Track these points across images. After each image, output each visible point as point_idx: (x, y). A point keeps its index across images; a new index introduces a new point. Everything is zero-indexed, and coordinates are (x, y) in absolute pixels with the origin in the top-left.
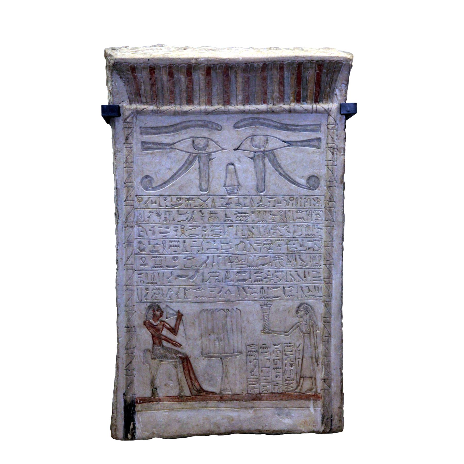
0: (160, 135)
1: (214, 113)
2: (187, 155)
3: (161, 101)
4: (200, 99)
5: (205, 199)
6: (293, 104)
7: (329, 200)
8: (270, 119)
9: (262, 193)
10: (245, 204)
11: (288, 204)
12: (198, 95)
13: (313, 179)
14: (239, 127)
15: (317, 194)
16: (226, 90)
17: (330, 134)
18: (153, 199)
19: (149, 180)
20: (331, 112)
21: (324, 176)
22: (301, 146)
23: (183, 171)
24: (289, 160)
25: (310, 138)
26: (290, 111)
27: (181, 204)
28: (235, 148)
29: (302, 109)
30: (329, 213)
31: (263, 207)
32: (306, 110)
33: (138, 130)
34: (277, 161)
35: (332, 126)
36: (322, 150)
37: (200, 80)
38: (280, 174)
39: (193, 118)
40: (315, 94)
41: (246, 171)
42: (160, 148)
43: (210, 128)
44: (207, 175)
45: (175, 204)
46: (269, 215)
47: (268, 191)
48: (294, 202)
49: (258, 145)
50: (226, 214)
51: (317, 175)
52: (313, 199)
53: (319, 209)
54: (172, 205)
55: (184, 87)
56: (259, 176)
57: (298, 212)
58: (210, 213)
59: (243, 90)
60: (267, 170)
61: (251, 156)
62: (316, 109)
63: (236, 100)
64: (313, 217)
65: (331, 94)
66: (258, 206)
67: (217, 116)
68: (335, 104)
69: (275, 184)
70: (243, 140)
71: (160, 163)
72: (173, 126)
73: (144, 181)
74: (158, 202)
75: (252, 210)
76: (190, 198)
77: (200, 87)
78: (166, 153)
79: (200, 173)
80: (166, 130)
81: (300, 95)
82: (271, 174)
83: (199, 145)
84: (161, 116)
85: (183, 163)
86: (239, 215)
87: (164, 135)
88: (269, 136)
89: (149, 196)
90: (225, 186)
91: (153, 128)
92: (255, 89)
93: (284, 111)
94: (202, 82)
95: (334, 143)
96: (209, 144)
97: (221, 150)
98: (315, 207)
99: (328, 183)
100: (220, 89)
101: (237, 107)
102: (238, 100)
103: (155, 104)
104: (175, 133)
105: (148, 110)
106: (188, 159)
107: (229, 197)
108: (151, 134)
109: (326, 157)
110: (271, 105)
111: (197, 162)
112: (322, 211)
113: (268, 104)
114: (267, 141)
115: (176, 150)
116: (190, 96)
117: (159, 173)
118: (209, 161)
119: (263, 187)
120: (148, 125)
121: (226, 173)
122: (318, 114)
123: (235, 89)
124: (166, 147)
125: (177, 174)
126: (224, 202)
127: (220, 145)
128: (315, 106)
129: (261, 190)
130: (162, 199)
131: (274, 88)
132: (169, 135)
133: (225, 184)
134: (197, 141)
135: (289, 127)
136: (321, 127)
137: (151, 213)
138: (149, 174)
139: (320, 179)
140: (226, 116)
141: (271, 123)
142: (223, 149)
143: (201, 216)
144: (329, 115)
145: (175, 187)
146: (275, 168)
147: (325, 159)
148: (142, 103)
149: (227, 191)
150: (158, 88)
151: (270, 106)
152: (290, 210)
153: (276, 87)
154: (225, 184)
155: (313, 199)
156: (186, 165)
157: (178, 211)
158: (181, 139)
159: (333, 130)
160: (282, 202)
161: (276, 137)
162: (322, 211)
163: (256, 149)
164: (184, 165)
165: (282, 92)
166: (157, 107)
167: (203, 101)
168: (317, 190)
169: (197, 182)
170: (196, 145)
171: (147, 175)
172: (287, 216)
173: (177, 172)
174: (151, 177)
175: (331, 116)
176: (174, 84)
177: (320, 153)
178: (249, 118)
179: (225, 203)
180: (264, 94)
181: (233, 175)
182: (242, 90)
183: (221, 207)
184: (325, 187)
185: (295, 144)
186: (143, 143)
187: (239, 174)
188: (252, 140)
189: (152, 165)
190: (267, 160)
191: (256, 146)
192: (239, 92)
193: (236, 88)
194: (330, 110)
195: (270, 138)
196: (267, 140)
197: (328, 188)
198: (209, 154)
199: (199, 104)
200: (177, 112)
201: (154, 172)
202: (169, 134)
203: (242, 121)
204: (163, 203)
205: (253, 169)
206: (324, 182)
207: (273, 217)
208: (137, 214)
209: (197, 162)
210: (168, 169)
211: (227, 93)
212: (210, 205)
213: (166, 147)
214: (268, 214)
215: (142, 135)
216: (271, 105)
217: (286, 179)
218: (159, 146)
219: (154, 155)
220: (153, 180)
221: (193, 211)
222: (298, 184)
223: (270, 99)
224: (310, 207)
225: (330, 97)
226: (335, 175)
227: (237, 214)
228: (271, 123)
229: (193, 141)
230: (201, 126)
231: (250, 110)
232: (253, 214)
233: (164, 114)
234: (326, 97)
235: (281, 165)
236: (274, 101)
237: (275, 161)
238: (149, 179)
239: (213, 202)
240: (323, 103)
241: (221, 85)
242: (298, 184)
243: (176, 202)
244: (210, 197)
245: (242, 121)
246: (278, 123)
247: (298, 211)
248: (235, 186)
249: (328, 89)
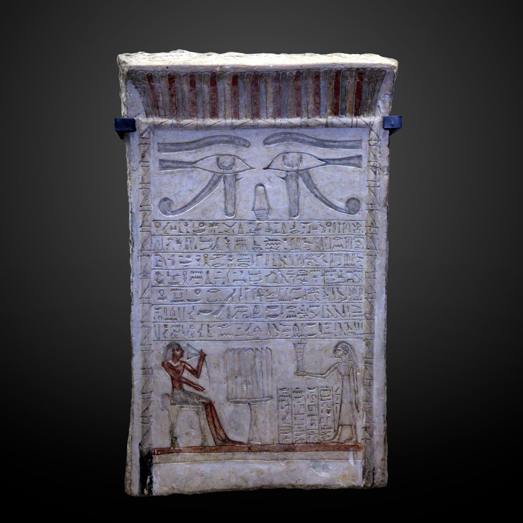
0: (181, 152)
1: (242, 128)
2: (210, 175)
3: (181, 114)
4: (225, 111)
5: (231, 224)
6: (330, 118)
7: (371, 225)
8: (305, 134)
9: (296, 218)
10: (276, 230)
11: (325, 230)
12: (223, 108)
13: (353, 202)
14: (269, 144)
15: (358, 219)
16: (255, 101)
17: (372, 151)
18: (173, 224)
19: (168, 203)
20: (373, 126)
22: (340, 165)
23: (206, 193)
25: (350, 156)
26: (327, 125)
27: (204, 230)
28: (264, 167)
29: (340, 123)
30: (371, 240)
31: (296, 233)
32: (345, 124)
33: (156, 146)
34: (312, 182)
35: (374, 142)
36: (363, 169)
37: (226, 90)
38: (316, 196)
39: (217, 133)
40: (355, 106)
41: (277, 193)
42: (181, 167)
43: (237, 145)
44: (233, 198)
45: (197, 230)
46: (303, 242)
47: (303, 215)
48: (331, 228)
49: (291, 163)
50: (254, 242)
51: (358, 197)
52: (353, 224)
53: (359, 236)
54: (194, 231)
55: (207, 98)
56: (292, 198)
57: (336, 239)
58: (236, 240)
59: (274, 101)
60: (300, 191)
61: (283, 175)
62: (357, 123)
63: (267, 113)
64: (352, 245)
65: (373, 105)
66: (291, 233)
67: (245, 131)
69: (310, 207)
70: (273, 157)
71: (180, 184)
72: (195, 142)
73: (162, 204)
74: (178, 228)
75: (284, 237)
76: (214, 223)
77: (225, 98)
78: (188, 173)
79: (225, 195)
80: (187, 147)
81: (339, 107)
82: (306, 196)
83: (224, 163)
84: (182, 131)
85: (206, 183)
86: (270, 242)
87: (185, 152)
88: (303, 153)
89: (168, 221)
90: (253, 209)
91: (172, 144)
92: (287, 100)
93: (320, 125)
94: (228, 92)
95: (376, 162)
96: (235, 162)
97: (249, 169)
98: (355, 234)
99: (370, 206)
100: (248, 100)
101: (267, 120)
102: (268, 112)
103: (175, 117)
104: (198, 150)
105: (167, 124)
106: (212, 179)
107: (258, 222)
108: (170, 151)
109: (368, 177)
110: (306, 118)
111: (222, 182)
112: (363, 237)
113: (302, 118)
114: (301, 159)
115: (199, 169)
116: (214, 108)
117: (180, 194)
118: (236, 181)
119: (297, 211)
120: (167, 141)
121: (255, 195)
122: (358, 129)
123: (265, 100)
124: (187, 166)
125: (200, 197)
126: (253, 227)
127: (248, 163)
128: (355, 119)
129: (294, 214)
130: (182, 224)
131: (309, 100)
132: (190, 153)
133: (254, 208)
134: (222, 159)
135: (326, 143)
136: (361, 144)
137: (170, 240)
138: (168, 197)
139: (361, 202)
140: (254, 131)
141: (306, 139)
142: (251, 168)
143: (227, 244)
144: (371, 129)
145: (197, 210)
146: (309, 189)
147: (367, 179)
148: (160, 116)
149: (256, 215)
150: (178, 99)
151: (305, 119)
152: (327, 237)
153: (311, 98)
154: (254, 208)
155: (353, 224)
156: (210, 186)
157: (201, 238)
158: (204, 156)
159: (375, 147)
160: (318, 228)
161: (311, 155)
162: (363, 237)
163: (288, 167)
164: (207, 186)
165: (317, 104)
166: (177, 121)
167: (229, 114)
168: (357, 214)
169: (223, 205)
170: (221, 163)
171: (166, 197)
172: (323, 244)
173: (199, 194)
174: (170, 200)
175: (373, 131)
176: (196, 95)
177: (361, 173)
178: (281, 133)
179: (254, 229)
180: (298, 106)
181: (263, 198)
182: (272, 102)
183: (249, 233)
184: (367, 211)
185: (332, 162)
186: (162, 161)
187: (270, 196)
188: (284, 158)
189: (171, 186)
190: (300, 181)
191: (289, 165)
192: (269, 104)
193: (266, 99)
194: (371, 124)
195: (304, 156)
196: (301, 158)
197: (370, 212)
198: (236, 174)
199: (225, 117)
200: (200, 126)
201: (173, 194)
202: (190, 151)
203: (272, 136)
204: (184, 229)
205: (286, 191)
207: (308, 244)
209: (222, 182)
210: (189, 190)
211: (256, 104)
212: (236, 231)
214: (302, 241)
215: (160, 152)
216: (306, 118)
217: (323, 201)
218: (180, 165)
219: (173, 175)
220: (173, 203)
221: (218, 238)
222: (336, 208)
223: (304, 112)
224: (350, 233)
225: (371, 109)
226: (378, 197)
227: (267, 241)
228: (306, 139)
229: (218, 159)
230: (227, 142)
231: (281, 124)
232: (285, 241)
233: (185, 128)
234: (367, 109)
235: (317, 186)
236: (309, 114)
237: (310, 181)
238: (168, 201)
239: (240, 227)
240: (364, 116)
241: (249, 96)
242: (336, 208)
243: (198, 228)
244: (236, 223)
245: (272, 136)
246: (314, 138)
247: (336, 238)
248: (265, 209)
249: (370, 101)
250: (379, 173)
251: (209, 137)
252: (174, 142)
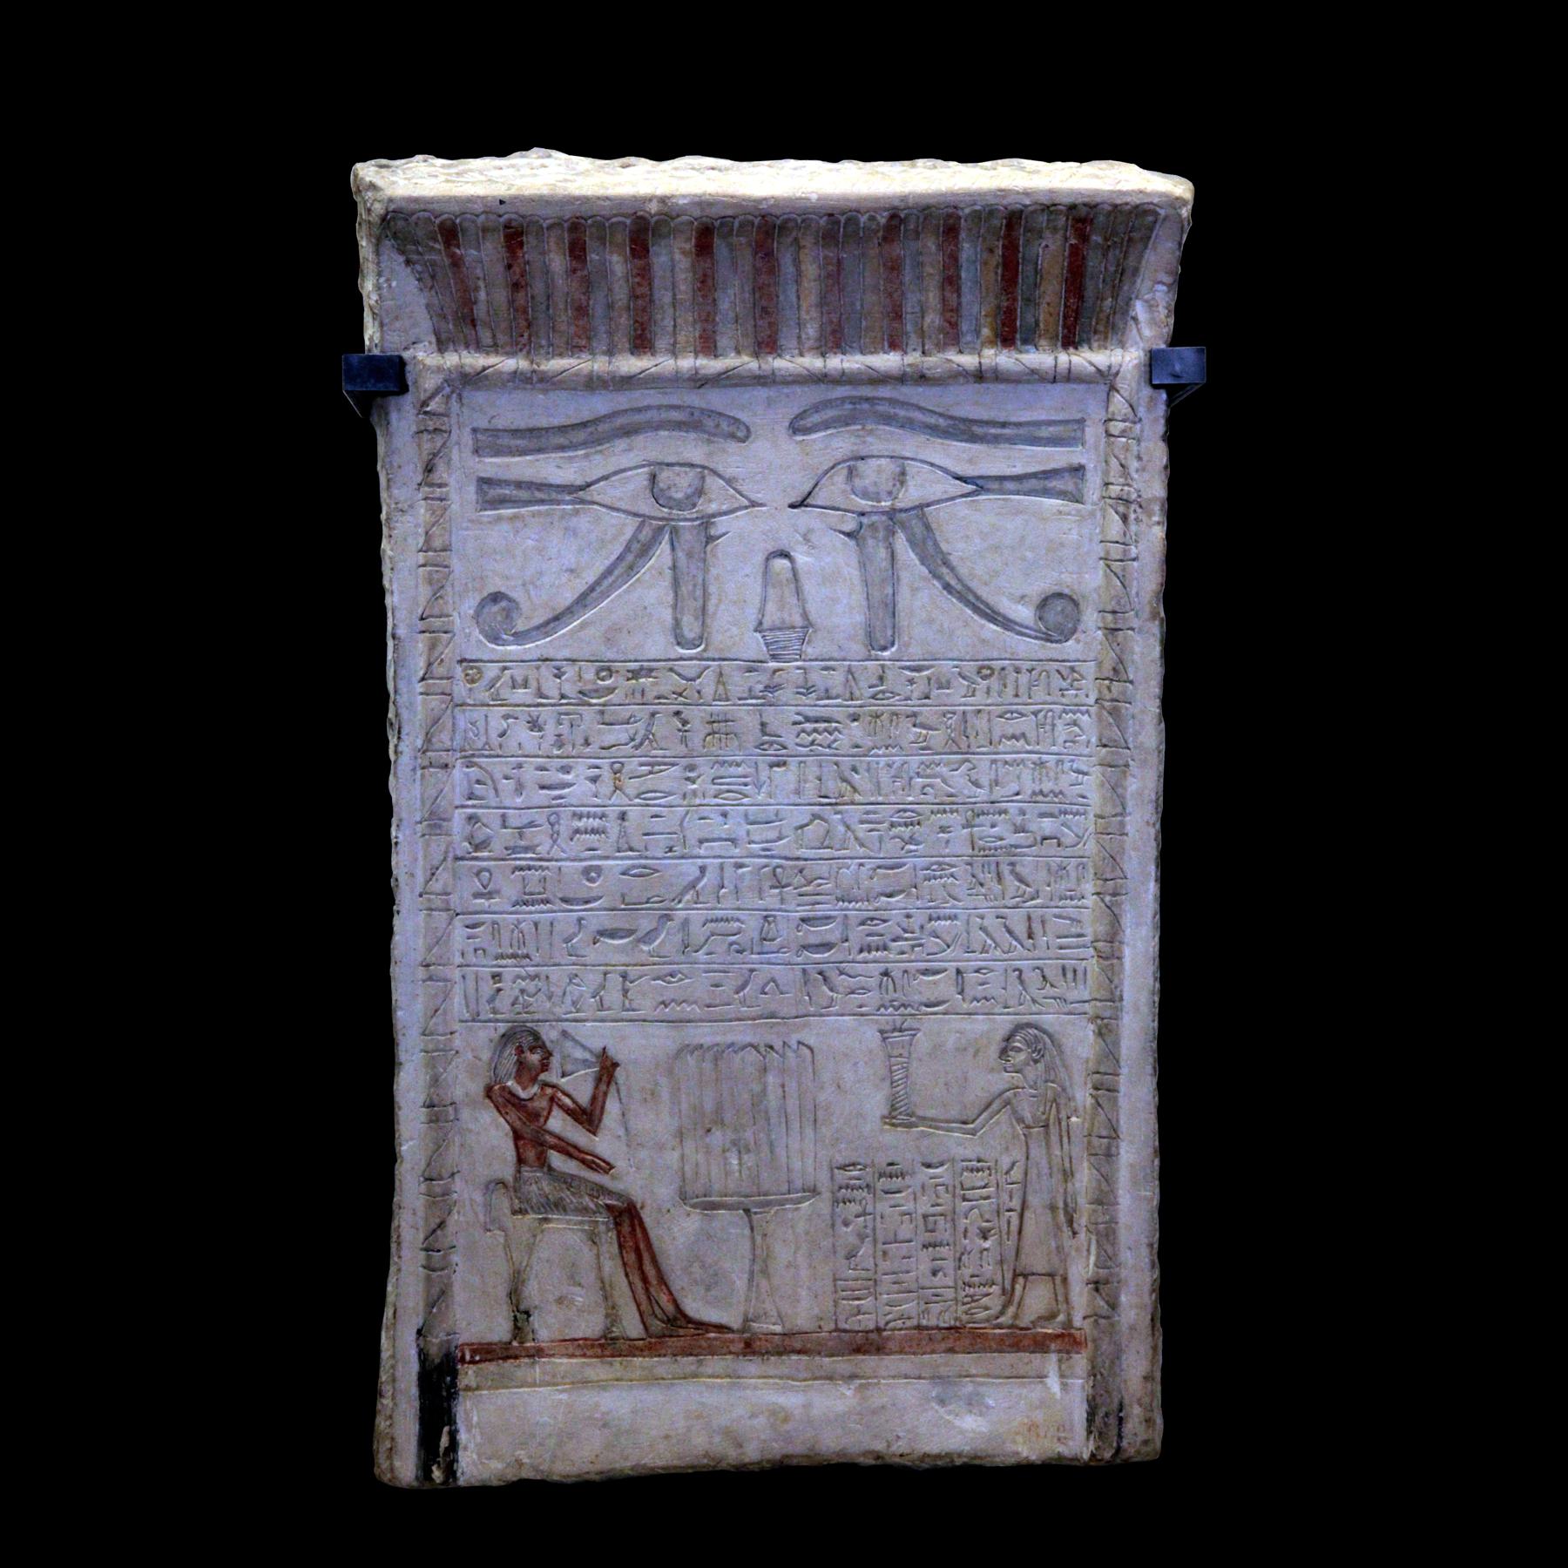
0: (542, 456)
1: (724, 382)
2: (631, 524)
3: (544, 342)
4: (675, 334)
5: (692, 673)
6: (989, 353)
7: (1111, 674)
8: (914, 401)
9: (886, 654)
10: (827, 691)
12: (669, 323)
13: (1059, 605)
14: (807, 431)
15: (1073, 657)
16: (764, 303)
17: (1116, 451)
18: (518, 672)
19: (504, 609)
20: (1118, 378)
22: (1018, 493)
23: (617, 578)
25: (1048, 467)
26: (980, 376)
27: (611, 690)
28: (793, 500)
29: (1019, 368)
30: (1111, 720)
31: (888, 698)
32: (1033, 372)
33: (467, 439)
34: (936, 544)
35: (1121, 425)
36: (1089, 507)
37: (677, 269)
38: (947, 587)
39: (652, 397)
40: (1065, 317)
41: (830, 578)
42: (542, 502)
43: (710, 434)
44: (699, 593)
45: (590, 691)
46: (910, 725)
47: (907, 645)
48: (994, 682)
49: (872, 489)
50: (763, 725)
51: (1072, 590)
52: (1058, 671)
53: (1078, 707)
54: (580, 692)
55: (621, 294)
56: (876, 595)
57: (1008, 715)
58: (709, 719)
59: (823, 303)
60: (901, 573)
61: (850, 526)
62: (1069, 370)
63: (799, 337)
64: (1056, 734)
65: (1118, 316)
66: (873, 697)
67: (734, 392)
68: (1132, 350)
69: (931, 621)
70: (820, 472)
71: (540, 551)
72: (584, 425)
73: (486, 610)
74: (533, 684)
75: (851, 710)
76: (642, 668)
78: (562, 517)
79: (676, 584)
80: (561, 440)
81: (1015, 319)
82: (917, 589)
83: (673, 489)
84: (545, 391)
85: (618, 549)
86: (808, 726)
87: (553, 455)
88: (908, 459)
89: (504, 663)
90: (759, 628)
91: (516, 432)
92: (862, 300)
93: (961, 375)
94: (683, 276)
95: (1128, 485)
96: (706, 487)
97: (746, 507)
98: (1064, 700)
99: (1109, 617)
100: (743, 301)
101: (800, 360)
102: (804, 336)
103: (524, 352)
104: (593, 450)
105: (500, 373)
106: (634, 538)
107: (773, 665)
108: (511, 452)
109: (1102, 531)
110: (917, 354)
111: (665, 546)
112: (1087, 711)
114: (901, 477)
115: (595, 507)
116: (642, 324)
117: (538, 583)
118: (707, 543)
119: (889, 633)
120: (500, 423)
121: (765, 585)
122: (1075, 386)
123: (794, 299)
124: (559, 497)
125: (598, 589)
126: (758, 681)
127: (744, 489)
128: (1063, 358)
129: (882, 642)
130: (546, 671)
131: (927, 299)
132: (570, 458)
133: (761, 623)
134: (665, 476)
135: (978, 430)
136: (1083, 431)
137: (510, 721)
138: (503, 590)
139: (1083, 606)
140: (762, 393)
141: (917, 415)
142: (754, 504)
143: (680, 730)
144: (1113, 388)
145: (591, 631)
146: (928, 567)
147: (1100, 537)
148: (479, 347)
149: (767, 645)
150: (533, 297)
151: (913, 358)
152: (979, 711)
153: (931, 295)
154: (761, 623)
155: (1058, 671)
156: (630, 557)
157: (602, 713)
158: (611, 469)
159: (1124, 440)
160: (954, 683)
161: (932, 465)
162: (1087, 711)
163: (864, 502)
164: (620, 558)
165: (952, 310)
166: (532, 363)
167: (687, 342)
168: (1070, 643)
169: (667, 615)
170: (662, 490)
171: (496, 590)
172: (969, 730)
173: (598, 582)
174: (510, 600)
175: (1118, 391)
176: (588, 285)
177: (1082, 518)
178: (843, 400)
179: (761, 687)
181: (789, 593)
182: (817, 306)
183: (746, 699)
184: (1100, 632)
185: (995, 486)
186: (485, 482)
187: (809, 587)
188: (851, 472)
189: (514, 557)
190: (901, 542)
191: (865, 495)
192: (808, 312)
193: (798, 298)
194: (1114, 370)
195: (912, 467)
196: (903, 473)
197: (1110, 637)
198: (706, 521)
199: (674, 352)
200: (599, 377)
201: (520, 582)
202: (571, 454)
203: (817, 408)
204: (551, 686)
205: (857, 573)
207: (924, 732)
208: (462, 723)
209: (665, 546)
210: (566, 571)
211: (767, 313)
212: (708, 691)
213: (559, 497)
214: (906, 723)
215: (479, 456)
216: (917, 354)
217: (968, 603)
218: (539, 495)
219: (519, 524)
220: (518, 608)
221: (653, 715)
222: (1007, 623)
223: (913, 335)
224: (1048, 698)
225: (1114, 327)
226: (1134, 592)
227: (800, 723)
228: (917, 415)
229: (653, 478)
230: (679, 426)
231: (843, 373)
232: (856, 724)
233: (554, 384)
234: (1101, 328)
235: (951, 558)
236: (926, 341)
237: (930, 543)
238: (504, 604)
239: (719, 682)
240: (1090, 348)
241: (746, 289)
242: (1007, 623)
243: (595, 683)
244: (708, 667)
245: (817, 408)
246: (941, 415)
247: (1006, 713)
248: (794, 627)
249: (1109, 302)
251: (626, 411)
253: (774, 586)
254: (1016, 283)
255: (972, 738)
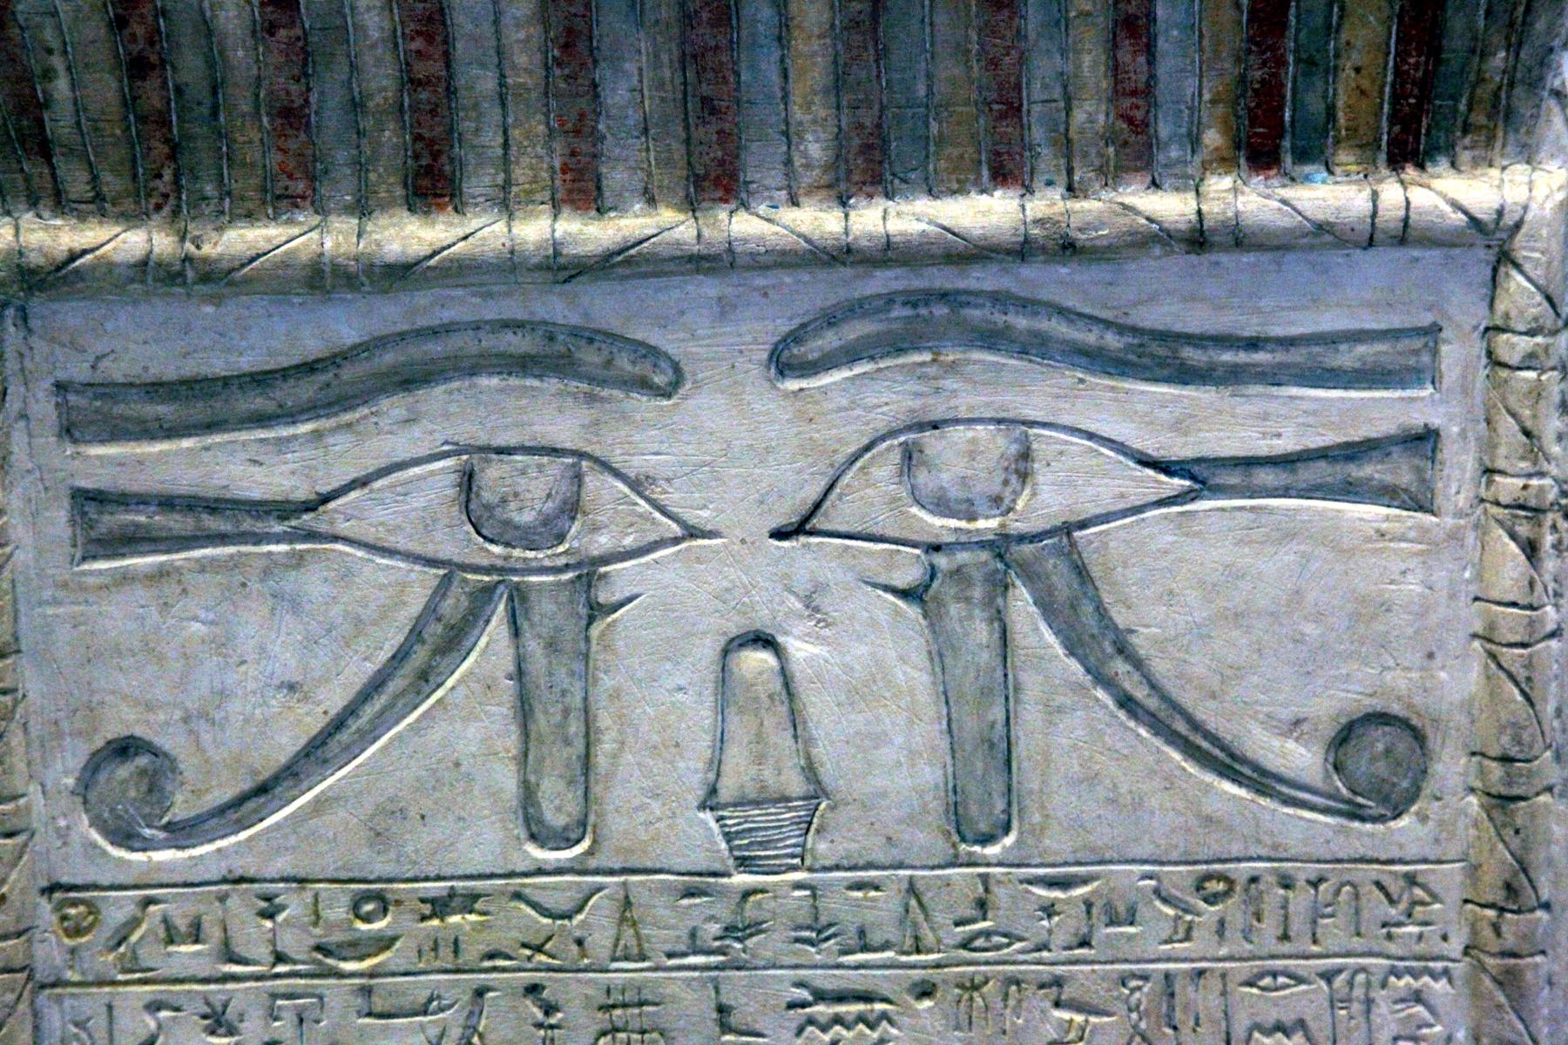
0: (218, 438)
1: (620, 270)
2: (420, 584)
3: (209, 189)
4: (506, 162)
5: (561, 902)
6: (1219, 184)
7: (1498, 896)
8: (1045, 295)
9: (992, 851)
10: (862, 933)
11: (1189, 929)
12: (491, 139)
13: (1379, 739)
14: (810, 368)
15: (1412, 851)
16: (705, 89)
17: (1512, 401)
18: (179, 910)
19: (143, 772)
20: (1520, 238)
21: (1463, 720)
22: (1285, 493)
23: (396, 697)
24: (1193, 597)
25: (1356, 435)
26: (1198, 239)
27: (385, 943)
28: (776, 522)
29: (1287, 221)
30: (1502, 999)
31: (998, 947)
32: (1322, 228)
33: (44, 407)
34: (1101, 611)
35: (1525, 344)
36: (1449, 521)
37: (506, 20)
38: (1126, 702)
39: (461, 306)
40: (1396, 98)
41: (858, 693)
42: (222, 539)
43: (591, 380)
44: (575, 727)
45: (340, 945)
46: (1047, 1004)
47: (1040, 831)
48: (1232, 907)
49: (954, 493)
50: (722, 1010)
51: (1410, 706)
52: (1379, 885)
53: (1423, 963)
54: (318, 948)
55: (381, 80)
56: (970, 725)
57: (1267, 981)
58: (603, 1000)
59: (838, 83)
60: (1024, 677)
61: (907, 576)
62: (1406, 220)
63: (788, 162)
64: (1377, 1020)
65: (1519, 91)
66: (966, 945)
67: (644, 290)
68: (1553, 166)
69: (1092, 779)
70: (840, 458)
71: (221, 644)
72: (309, 368)
73: (102, 777)
74: (213, 933)
75: (917, 974)
76: (452, 893)
77: (503, 76)
78: (266, 573)
79: (524, 711)
80: (258, 402)
81: (1281, 108)
82: (1060, 710)
83: (513, 506)
84: (217, 300)
85: (393, 639)
86: (822, 1010)
87: (244, 436)
88: (1033, 424)
89: (147, 888)
90: (710, 800)
91: (156, 389)
92: (929, 76)
93: (1159, 238)
94: (522, 35)
95: (1542, 474)
96: (586, 497)
97: (676, 541)
98: (1393, 948)
99: (1496, 770)
100: (660, 85)
101: (789, 215)
102: (798, 161)
103: (166, 210)
104: (331, 423)
105: (110, 266)
106: (431, 610)
107: (742, 879)
108: (147, 431)
109: (1479, 577)
110: (1056, 193)
111: (497, 626)
112: (1446, 972)
113: (1029, 190)
114: (1022, 465)
115: (339, 547)
116: (431, 143)
117: (218, 716)
118: (591, 620)
119: (1000, 805)
120: (117, 370)
121: (722, 709)
122: (1416, 253)
123: (776, 78)
124: (259, 527)
125: (354, 725)
126: (709, 917)
127: (672, 497)
128: (1392, 194)
129: (983, 827)
130: (241, 905)
131: (1079, 67)
132: (280, 441)
133: (713, 791)
134: (493, 475)
135: (1191, 355)
136: (1435, 353)
137: (164, 1014)
138: (138, 731)
139: (1433, 741)
140: (711, 288)
141: (1058, 328)
142: (693, 532)
143: (539, 1026)
144: (1504, 258)
145: (338, 816)
146: (1083, 661)
147: (1474, 589)
148: (61, 203)
149: (728, 837)
150: (179, 90)
151: (1047, 203)
152: (1201, 973)
153: (1087, 60)
154: (713, 791)
155: (1379, 885)
156: (420, 656)
157: (367, 991)
158: (372, 465)
159: (1532, 375)
160: (1143, 912)
161: (1091, 436)
162: (1446, 972)
163: (938, 521)
164: (400, 656)
165: (1134, 93)
166: (183, 239)
167: (534, 180)
168: (1404, 822)
169: (507, 780)
170: (488, 507)
171: (127, 733)
172: (1178, 1015)
173: (351, 710)
174: (155, 752)
175: (1518, 266)
176: (304, 59)
177: (1432, 547)
178: (890, 300)
179: (715, 928)
180: (1002, 116)
181: (774, 720)
182: (826, 91)
183: (684, 955)
184: (1473, 800)
185: (1234, 478)
186: (88, 500)
187: (819, 708)
188: (910, 456)
189: (161, 659)
190: (1022, 601)
191: (941, 505)
192: (808, 106)
193: (785, 75)
194: (1509, 220)
195: (1045, 443)
196: (1026, 455)
197: (1496, 814)
198: (588, 572)
199: (506, 203)
200: (336, 267)
201: (178, 714)
202: (285, 432)
203: (830, 319)
204: (253, 935)
205: (925, 678)
206: (1463, 761)
207: (1079, 1018)
208: (54, 1019)
209: (497, 626)
210: (281, 686)
211: (714, 111)
212: (601, 942)
213: (259, 527)
214: (1040, 1001)
215: (75, 441)
216: (1056, 193)
217: (1174, 739)
218: (224, 526)
219: (170, 588)
220: (174, 770)
221: (480, 993)
222: (1262, 780)
223: (1045, 151)
224: (1357, 943)
225: (1509, 114)
226: (1550, 708)
227: (804, 1005)
228: (1058, 328)
229: (468, 479)
230: (523, 365)
231: (888, 243)
232: (927, 1003)
233: (231, 284)
234: (1479, 118)
235: (1134, 639)
236: (1076, 164)
237: (1087, 608)
238: (143, 761)
239: (622, 920)
240: (1453, 165)
241: (665, 58)
242: (1262, 780)
243: (352, 929)
244: (600, 888)
245: (830, 319)
246: (1108, 324)
247: (1262, 976)
248: (788, 800)
249: (1500, 57)
250: (1557, 546)
251: (402, 336)
252: (171, 374)
253: (741, 711)
254: (1284, 26)
255: (1186, 1031)
